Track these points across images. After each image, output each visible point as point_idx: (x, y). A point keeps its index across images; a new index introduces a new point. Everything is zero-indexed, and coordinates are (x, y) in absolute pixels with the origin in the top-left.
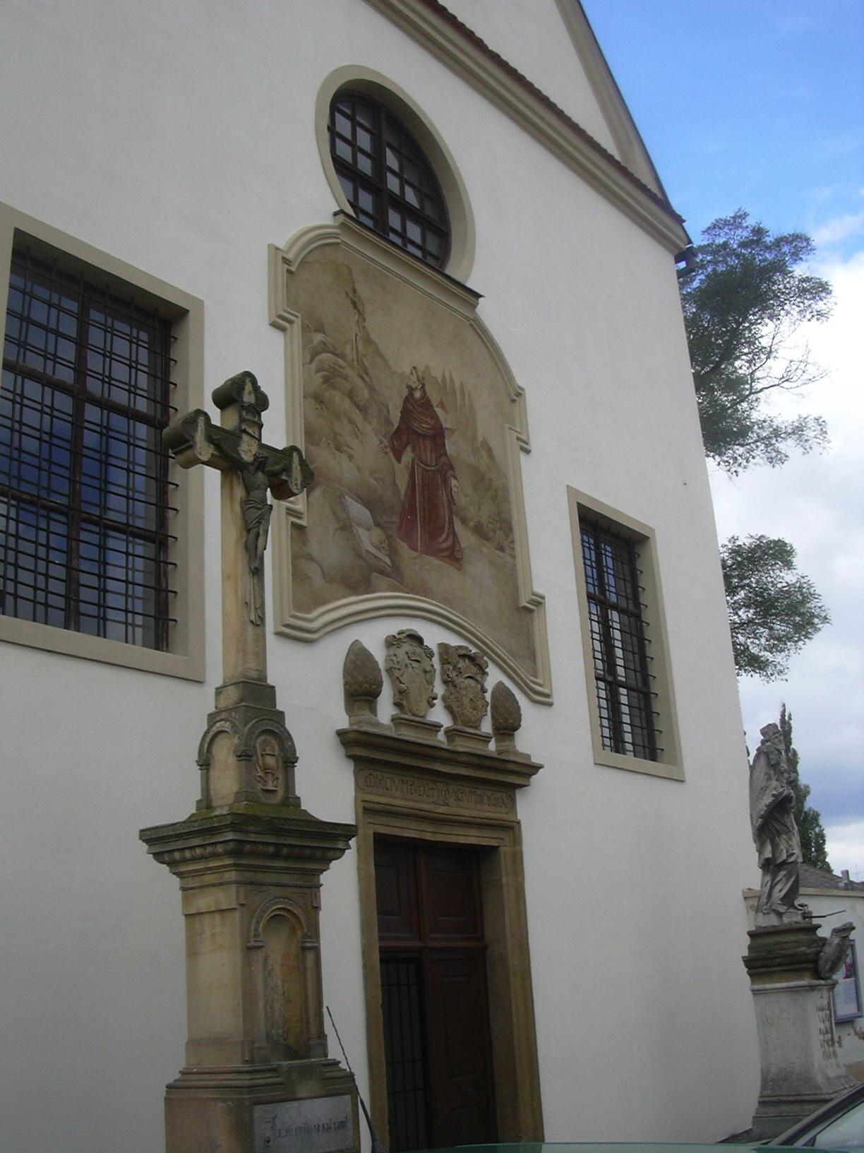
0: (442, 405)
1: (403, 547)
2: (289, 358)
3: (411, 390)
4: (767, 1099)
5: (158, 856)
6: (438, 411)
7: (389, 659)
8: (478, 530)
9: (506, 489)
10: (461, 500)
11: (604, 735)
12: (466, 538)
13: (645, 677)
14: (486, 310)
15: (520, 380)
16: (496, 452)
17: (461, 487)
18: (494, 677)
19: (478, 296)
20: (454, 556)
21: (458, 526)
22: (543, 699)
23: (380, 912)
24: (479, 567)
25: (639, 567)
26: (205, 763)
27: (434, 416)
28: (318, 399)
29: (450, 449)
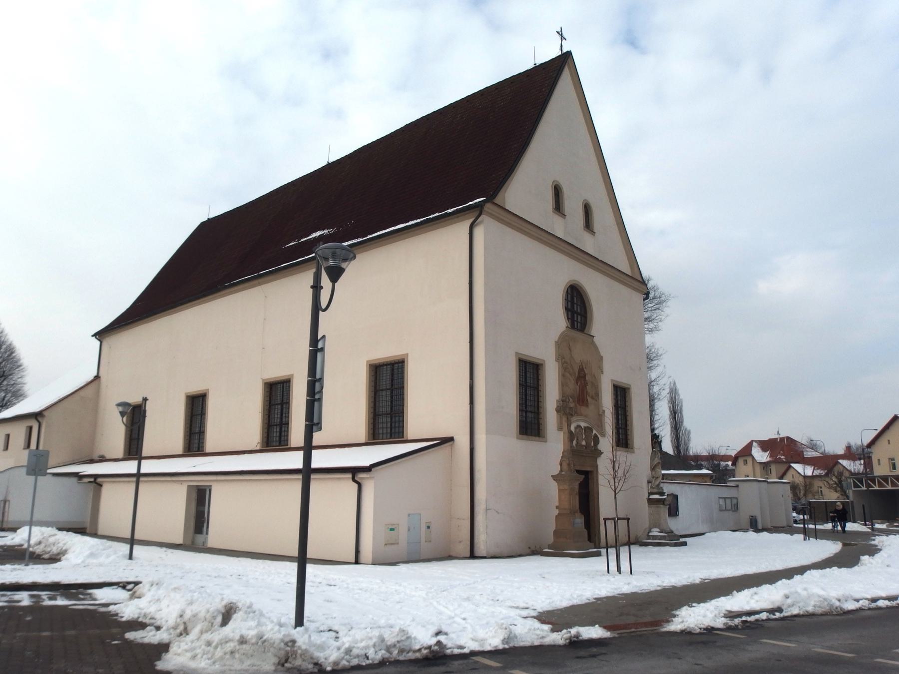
0: (586, 368)
1: (578, 405)
2: (559, 365)
3: (580, 366)
4: (524, 432)
5: (554, 480)
6: (585, 369)
7: (575, 431)
8: (592, 398)
9: (598, 386)
10: (589, 391)
11: (625, 521)
12: (589, 399)
13: (626, 425)
14: (595, 339)
15: (602, 354)
16: (597, 377)
17: (589, 387)
18: (594, 432)
19: (593, 336)
20: (587, 405)
21: (588, 398)
22: (603, 435)
23: (403, 387)
24: (592, 407)
25: (628, 433)
26: (561, 465)
27: (584, 371)
28: (563, 375)
29: (587, 378)
